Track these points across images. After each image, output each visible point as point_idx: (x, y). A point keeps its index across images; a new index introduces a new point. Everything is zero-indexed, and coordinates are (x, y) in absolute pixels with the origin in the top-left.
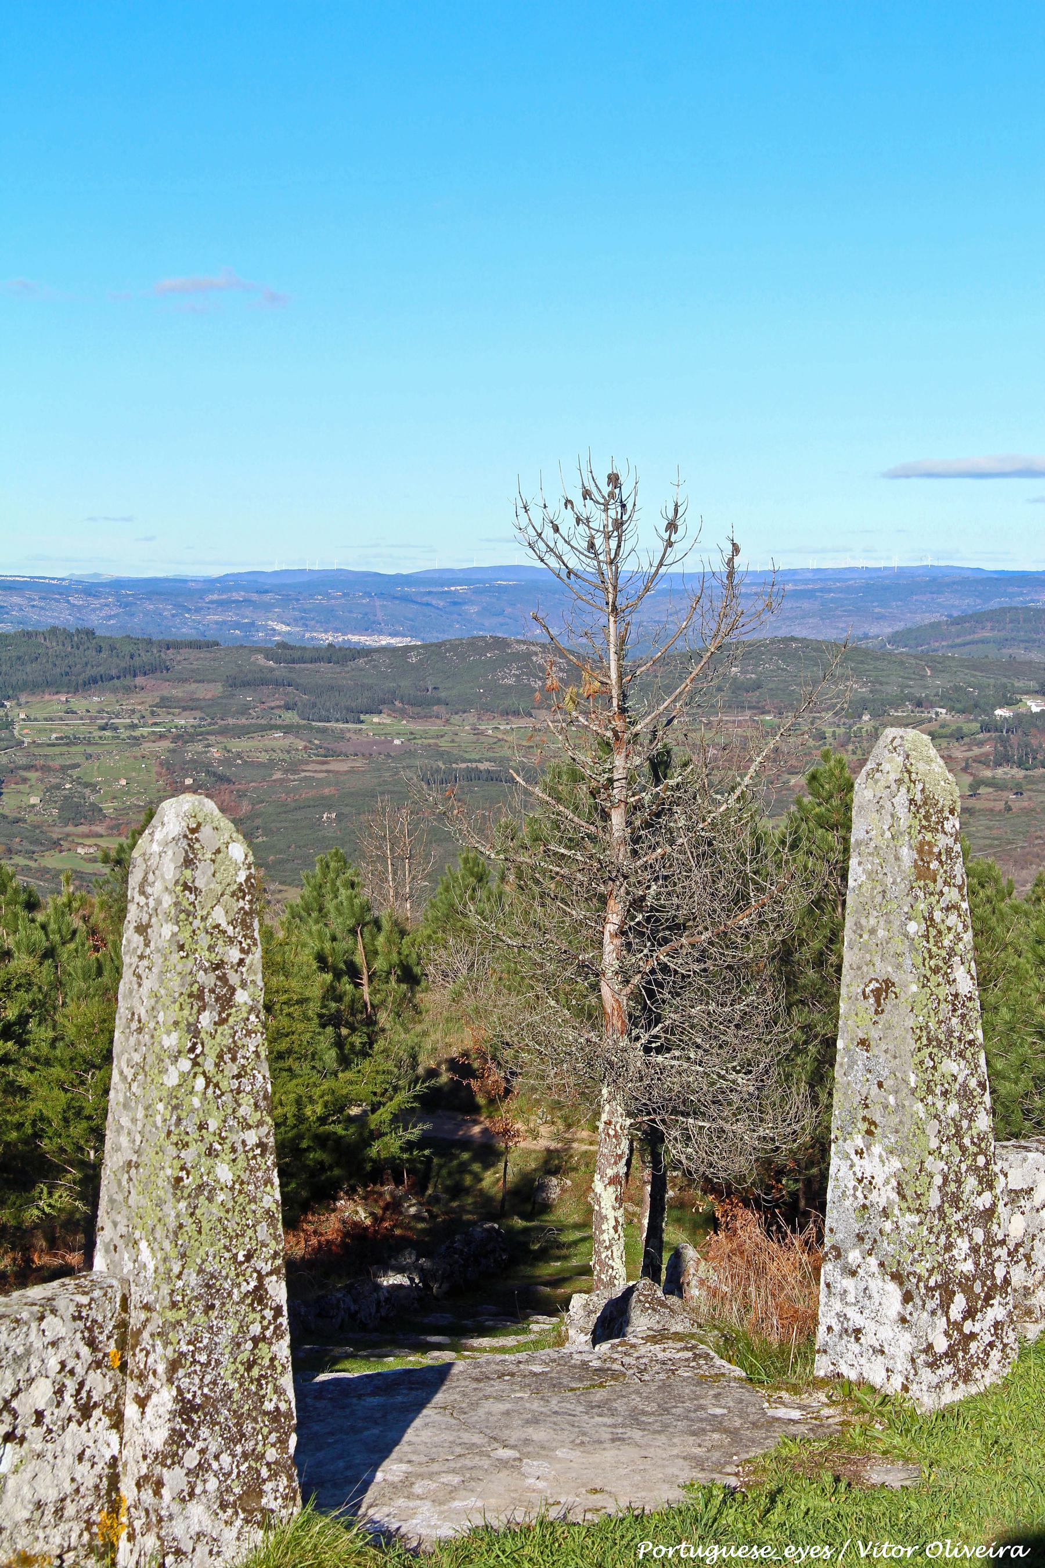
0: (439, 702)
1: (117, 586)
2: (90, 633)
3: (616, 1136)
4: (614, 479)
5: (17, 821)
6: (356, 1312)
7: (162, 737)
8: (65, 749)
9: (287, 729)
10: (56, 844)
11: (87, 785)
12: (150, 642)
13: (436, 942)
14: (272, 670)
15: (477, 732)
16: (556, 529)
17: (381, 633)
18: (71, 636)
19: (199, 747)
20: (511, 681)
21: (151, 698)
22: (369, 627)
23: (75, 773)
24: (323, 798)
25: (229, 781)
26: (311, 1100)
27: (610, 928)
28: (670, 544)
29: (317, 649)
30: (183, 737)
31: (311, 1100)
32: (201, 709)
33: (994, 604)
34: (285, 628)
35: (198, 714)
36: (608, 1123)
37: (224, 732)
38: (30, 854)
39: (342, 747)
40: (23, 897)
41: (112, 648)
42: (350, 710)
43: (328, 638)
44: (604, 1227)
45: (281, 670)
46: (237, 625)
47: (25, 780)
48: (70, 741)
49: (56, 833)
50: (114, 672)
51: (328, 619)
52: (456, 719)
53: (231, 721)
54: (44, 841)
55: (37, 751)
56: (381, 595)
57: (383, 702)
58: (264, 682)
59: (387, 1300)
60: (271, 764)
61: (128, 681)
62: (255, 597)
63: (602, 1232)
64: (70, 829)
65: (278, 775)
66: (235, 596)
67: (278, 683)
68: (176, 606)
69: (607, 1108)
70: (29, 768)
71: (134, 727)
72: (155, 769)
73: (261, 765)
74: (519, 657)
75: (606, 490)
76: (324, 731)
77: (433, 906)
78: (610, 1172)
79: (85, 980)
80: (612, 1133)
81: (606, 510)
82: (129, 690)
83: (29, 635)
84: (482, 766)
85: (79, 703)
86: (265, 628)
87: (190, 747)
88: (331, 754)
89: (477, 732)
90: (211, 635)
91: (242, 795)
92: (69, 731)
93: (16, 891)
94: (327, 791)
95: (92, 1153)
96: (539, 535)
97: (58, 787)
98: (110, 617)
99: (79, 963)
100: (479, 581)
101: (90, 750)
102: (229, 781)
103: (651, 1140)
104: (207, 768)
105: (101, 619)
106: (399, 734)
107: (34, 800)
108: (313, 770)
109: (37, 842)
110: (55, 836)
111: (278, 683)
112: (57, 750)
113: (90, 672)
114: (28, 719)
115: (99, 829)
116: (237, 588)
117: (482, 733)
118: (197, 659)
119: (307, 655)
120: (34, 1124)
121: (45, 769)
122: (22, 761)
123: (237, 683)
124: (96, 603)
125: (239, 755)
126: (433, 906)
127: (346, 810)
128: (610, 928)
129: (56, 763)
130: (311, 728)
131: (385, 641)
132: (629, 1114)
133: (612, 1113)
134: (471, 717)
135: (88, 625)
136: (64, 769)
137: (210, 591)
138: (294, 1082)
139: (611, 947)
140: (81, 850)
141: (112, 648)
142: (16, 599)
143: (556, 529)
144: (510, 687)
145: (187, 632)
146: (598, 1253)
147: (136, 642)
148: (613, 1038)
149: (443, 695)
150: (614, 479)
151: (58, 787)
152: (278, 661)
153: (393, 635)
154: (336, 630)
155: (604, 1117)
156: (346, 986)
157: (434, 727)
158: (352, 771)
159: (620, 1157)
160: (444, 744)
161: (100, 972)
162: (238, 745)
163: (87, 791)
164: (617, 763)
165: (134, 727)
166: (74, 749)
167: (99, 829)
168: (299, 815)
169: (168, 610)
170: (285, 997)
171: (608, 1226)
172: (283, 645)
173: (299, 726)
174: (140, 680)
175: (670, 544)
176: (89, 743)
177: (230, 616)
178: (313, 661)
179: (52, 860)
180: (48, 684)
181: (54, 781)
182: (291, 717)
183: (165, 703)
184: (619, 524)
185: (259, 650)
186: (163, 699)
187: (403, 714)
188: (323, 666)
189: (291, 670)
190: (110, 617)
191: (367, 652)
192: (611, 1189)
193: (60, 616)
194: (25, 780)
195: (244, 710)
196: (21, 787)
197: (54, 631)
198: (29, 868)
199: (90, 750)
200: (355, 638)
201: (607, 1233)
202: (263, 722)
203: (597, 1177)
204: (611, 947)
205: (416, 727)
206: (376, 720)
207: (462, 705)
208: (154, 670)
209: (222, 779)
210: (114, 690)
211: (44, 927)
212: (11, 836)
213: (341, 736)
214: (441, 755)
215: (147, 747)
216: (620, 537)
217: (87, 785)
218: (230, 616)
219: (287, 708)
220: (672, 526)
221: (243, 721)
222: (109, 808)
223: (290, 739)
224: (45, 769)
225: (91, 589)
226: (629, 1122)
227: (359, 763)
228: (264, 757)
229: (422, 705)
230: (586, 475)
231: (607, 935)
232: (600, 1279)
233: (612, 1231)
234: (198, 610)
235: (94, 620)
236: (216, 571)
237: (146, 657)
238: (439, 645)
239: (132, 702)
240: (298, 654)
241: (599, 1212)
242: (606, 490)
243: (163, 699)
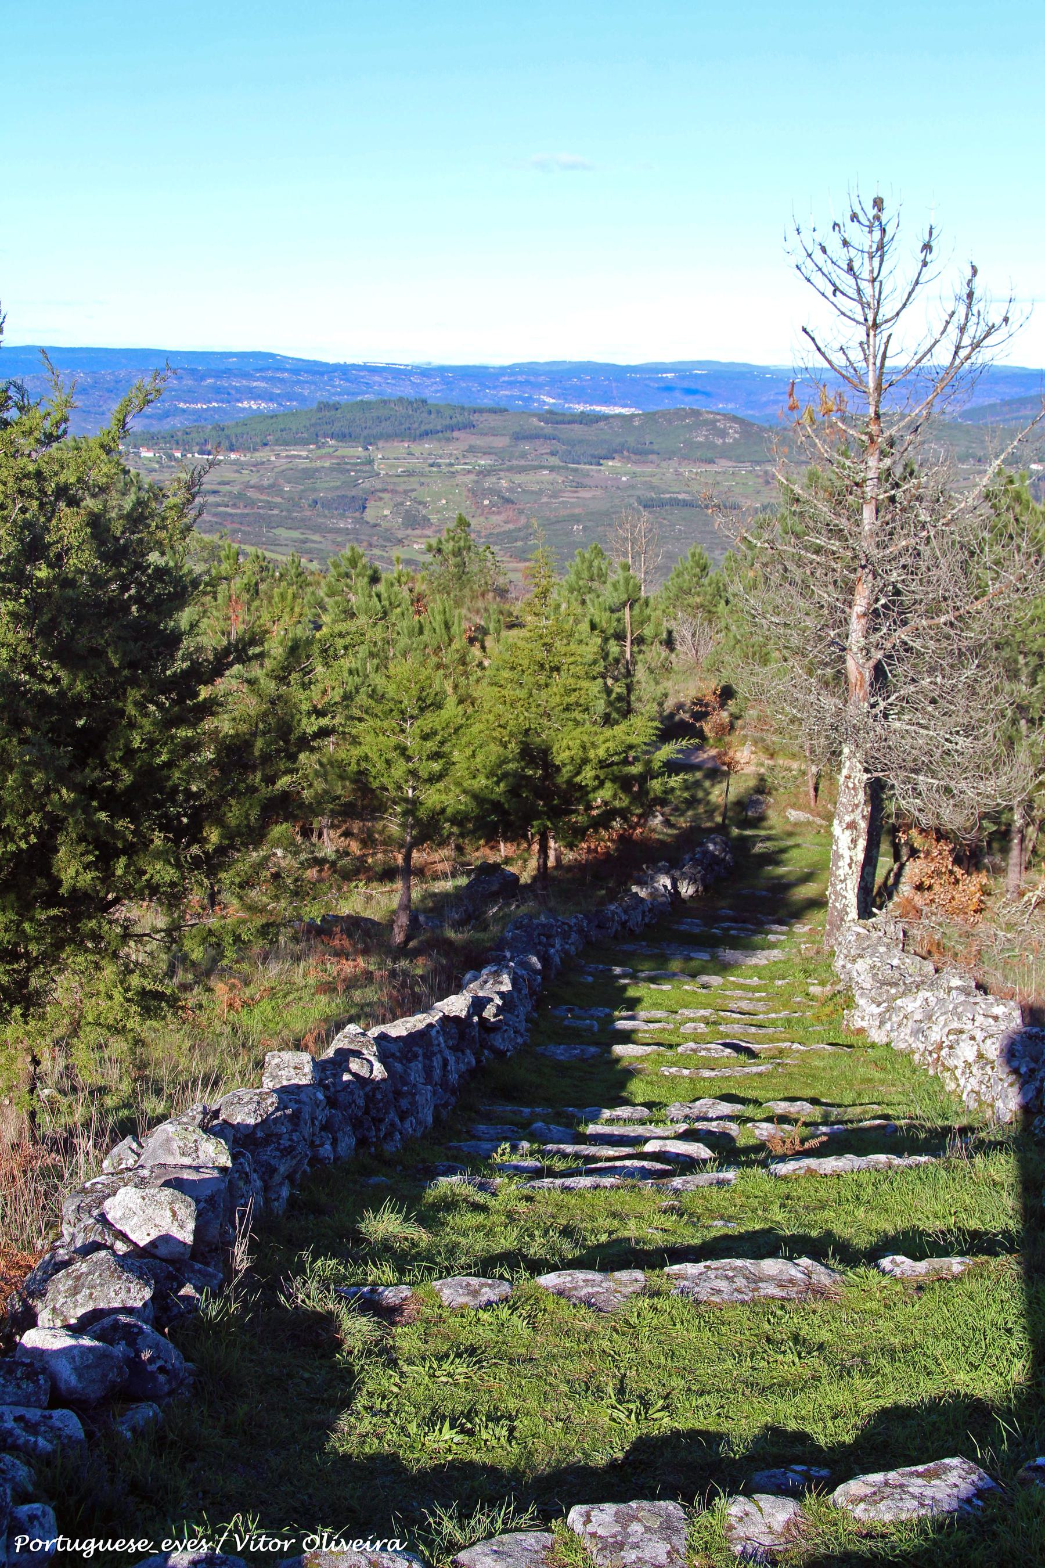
0: (652, 452)
1: (442, 370)
2: (424, 402)
3: (854, 788)
4: (878, 203)
5: (375, 526)
6: (626, 921)
7: (469, 472)
8: (406, 479)
9: (552, 469)
10: (400, 541)
11: (420, 503)
12: (463, 408)
13: (668, 615)
14: (542, 429)
15: (677, 473)
16: (824, 250)
17: (615, 405)
18: (411, 403)
19: (494, 479)
20: (701, 439)
21: (463, 446)
22: (607, 401)
23: (413, 495)
24: (573, 515)
25: (513, 502)
26: (594, 745)
27: (859, 608)
28: (925, 264)
29: (572, 415)
30: (484, 473)
31: (594, 745)
32: (495, 454)
33: (1033, 392)
34: (552, 401)
35: (493, 457)
36: (848, 777)
37: (510, 469)
38: (383, 548)
39: (587, 481)
40: (369, 572)
41: (438, 412)
42: (593, 456)
43: (579, 408)
44: (840, 864)
45: (548, 429)
46: (521, 398)
47: (381, 499)
48: (410, 474)
49: (400, 535)
50: (439, 428)
51: (580, 395)
52: (664, 464)
53: (515, 462)
54: (392, 540)
55: (389, 480)
56: (616, 380)
57: (616, 451)
58: (537, 437)
59: (650, 910)
60: (540, 493)
61: (448, 434)
62: (532, 379)
63: (838, 868)
64: (409, 532)
65: (545, 500)
66: (520, 378)
67: (546, 437)
68: (480, 384)
69: (848, 764)
70: (384, 490)
71: (451, 465)
72: (465, 493)
73: (533, 492)
74: (706, 423)
75: (872, 212)
76: (576, 470)
77: (667, 589)
78: (848, 819)
79: (410, 637)
80: (851, 785)
81: (871, 232)
82: (448, 440)
83: (385, 402)
84: (680, 497)
85: (416, 448)
86: (538, 400)
87: (488, 479)
88: (580, 486)
89: (677, 473)
90: (503, 404)
91: (521, 512)
92: (410, 468)
93: (364, 566)
94: (577, 511)
95: (410, 791)
96: (810, 255)
97: (402, 504)
98: (437, 392)
99: (405, 623)
100: (685, 371)
101: (422, 480)
102: (513, 502)
103: (876, 790)
104: (498, 493)
105: (433, 393)
106: (625, 474)
107: (386, 512)
108: (567, 497)
109: (389, 540)
110: (400, 536)
111: (546, 437)
112: (401, 479)
113: (423, 428)
114: (383, 458)
115: (428, 532)
116: (521, 373)
117: (681, 474)
118: (493, 421)
119: (566, 419)
120: (358, 764)
121: (394, 492)
122: (379, 486)
123: (519, 437)
124: (428, 382)
125: (520, 486)
126: (667, 589)
127: (589, 524)
128: (859, 608)
129: (400, 489)
130: (568, 468)
131: (618, 410)
132: (867, 770)
133: (851, 768)
134: (674, 463)
135: (423, 397)
136: (406, 492)
137: (503, 375)
138: (579, 730)
139: (857, 627)
140: (415, 546)
141: (438, 412)
142: (377, 378)
143: (824, 250)
144: (700, 443)
145: (487, 403)
146: (834, 885)
147: (454, 408)
148: (859, 702)
149: (655, 447)
150: (878, 203)
151: (402, 504)
152: (547, 423)
153: (623, 406)
154: (586, 403)
155: (845, 772)
156: (614, 648)
157: (649, 469)
158: (594, 498)
159: (857, 806)
160: (655, 481)
161: (421, 632)
162: (519, 479)
163: (421, 507)
164: (870, 464)
165: (451, 465)
166: (412, 479)
167: (428, 532)
168: (558, 527)
169: (475, 387)
170: (572, 659)
171: (844, 863)
172: (551, 412)
173: (559, 467)
174: (456, 434)
175: (925, 264)
176: (423, 475)
177: (516, 392)
178: (570, 422)
179: (396, 552)
180: (396, 435)
181: (400, 500)
182: (554, 461)
183: (472, 450)
184: (881, 247)
185: (535, 415)
186: (471, 447)
187: (629, 459)
188: (576, 426)
189: (556, 429)
190: (437, 392)
191: (606, 418)
192: (848, 833)
193: (407, 391)
194: (381, 499)
195: (523, 455)
196: (379, 503)
197: (401, 400)
198: (382, 557)
199: (422, 480)
200: (598, 408)
201: (843, 869)
202: (535, 463)
203: (836, 822)
204: (857, 627)
205: (638, 469)
206: (610, 463)
207: (669, 455)
208: (465, 428)
209: (508, 501)
210: (439, 440)
211: (378, 596)
212: (371, 536)
213: (587, 475)
214: (653, 488)
215: (460, 479)
216: (882, 257)
217: (420, 503)
218: (516, 392)
219: (553, 454)
220: (927, 247)
221: (523, 462)
222: (434, 518)
223: (554, 475)
224: (394, 492)
225: (426, 372)
226: (866, 776)
227: (599, 493)
228: (536, 488)
229: (641, 453)
230: (855, 201)
231: (854, 616)
232: (835, 907)
233: (847, 868)
234: (495, 388)
235: (427, 393)
236: (507, 362)
237: (460, 419)
238: (655, 414)
239: (450, 448)
240: (560, 418)
241: (836, 852)
242: (872, 212)
243: (471, 447)
